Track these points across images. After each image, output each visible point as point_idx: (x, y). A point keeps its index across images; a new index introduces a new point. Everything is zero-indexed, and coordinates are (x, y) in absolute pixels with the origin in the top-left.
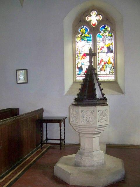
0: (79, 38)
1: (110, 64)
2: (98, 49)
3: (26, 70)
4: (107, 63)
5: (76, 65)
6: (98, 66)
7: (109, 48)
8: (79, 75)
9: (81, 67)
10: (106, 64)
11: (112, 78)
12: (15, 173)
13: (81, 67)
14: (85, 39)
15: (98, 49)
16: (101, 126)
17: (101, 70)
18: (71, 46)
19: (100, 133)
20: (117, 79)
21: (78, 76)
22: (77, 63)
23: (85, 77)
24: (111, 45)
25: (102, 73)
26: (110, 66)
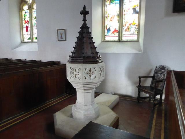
0: (109, 2)
1: (135, 25)
2: (124, 11)
3: (65, 30)
4: (131, 24)
5: (106, 27)
6: (123, 27)
7: (134, 9)
8: (108, 35)
9: (109, 28)
10: (131, 25)
11: (135, 38)
12: (30, 114)
13: (109, 28)
14: (114, 3)
15: (124, 11)
16: (92, 83)
17: (126, 30)
18: (100, 10)
19: (92, 89)
20: (139, 39)
21: (107, 36)
22: (106, 25)
23: (36, 11)
24: (137, 6)
25: (127, 33)
26: (135, 27)
